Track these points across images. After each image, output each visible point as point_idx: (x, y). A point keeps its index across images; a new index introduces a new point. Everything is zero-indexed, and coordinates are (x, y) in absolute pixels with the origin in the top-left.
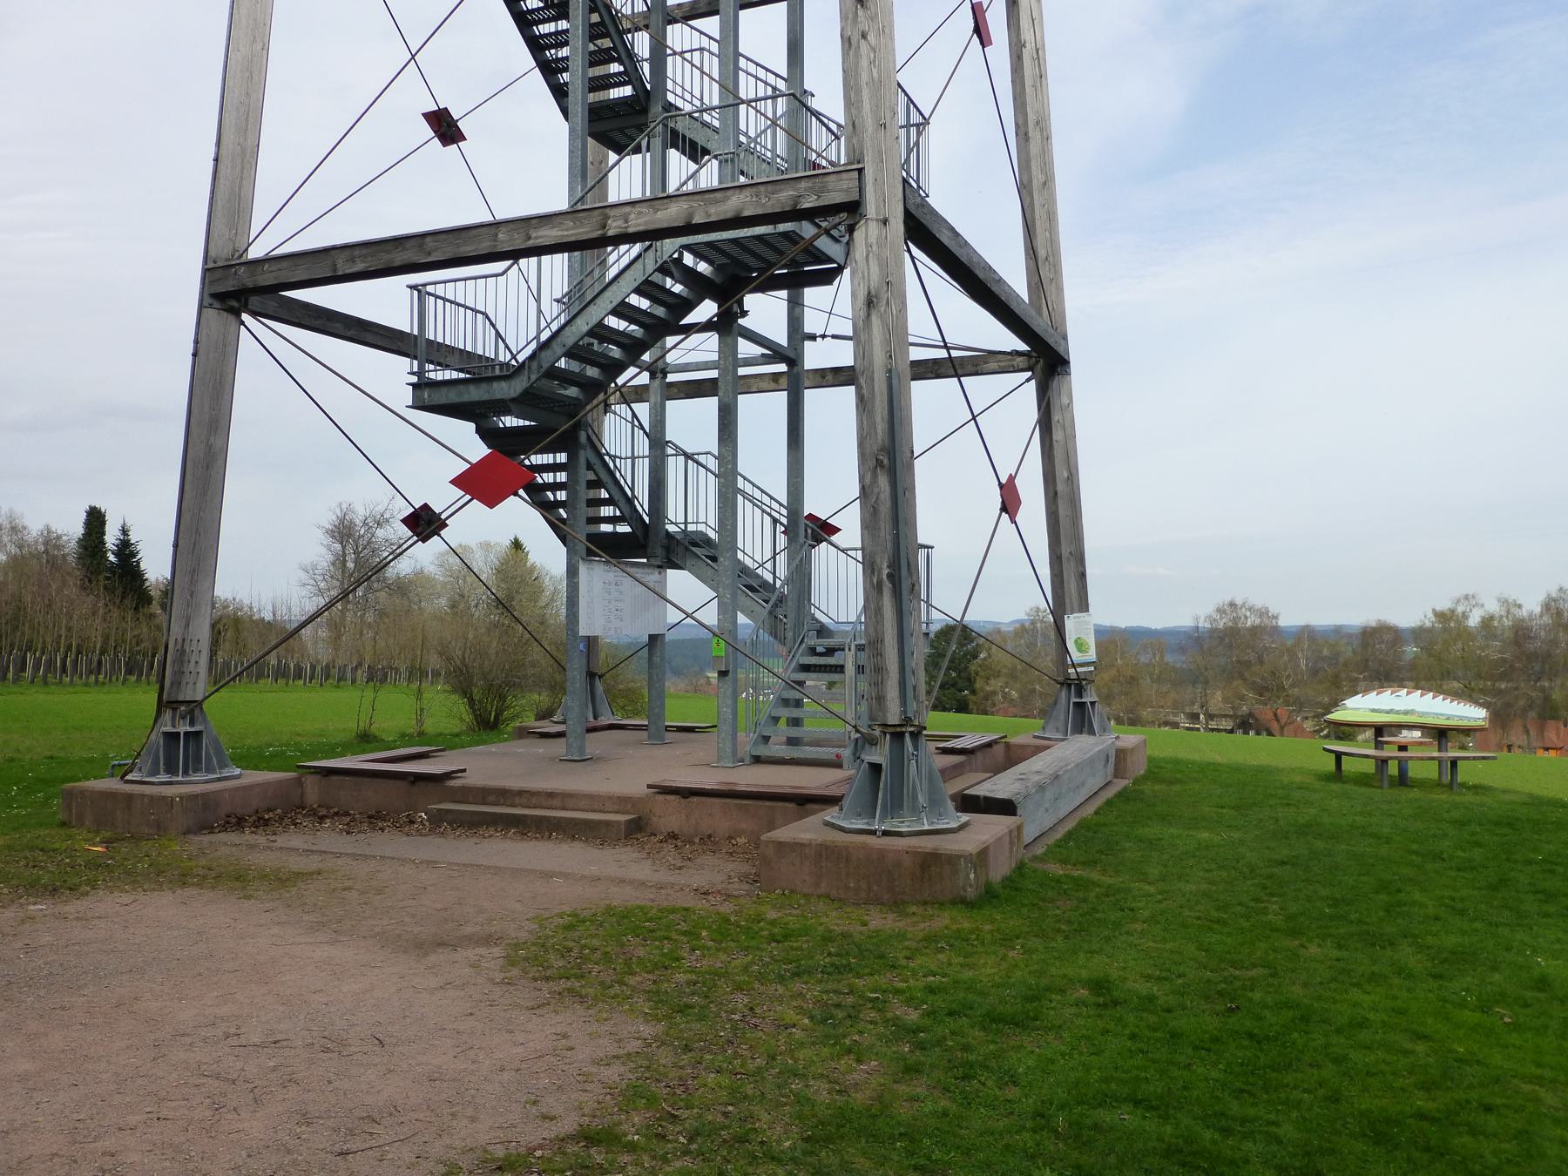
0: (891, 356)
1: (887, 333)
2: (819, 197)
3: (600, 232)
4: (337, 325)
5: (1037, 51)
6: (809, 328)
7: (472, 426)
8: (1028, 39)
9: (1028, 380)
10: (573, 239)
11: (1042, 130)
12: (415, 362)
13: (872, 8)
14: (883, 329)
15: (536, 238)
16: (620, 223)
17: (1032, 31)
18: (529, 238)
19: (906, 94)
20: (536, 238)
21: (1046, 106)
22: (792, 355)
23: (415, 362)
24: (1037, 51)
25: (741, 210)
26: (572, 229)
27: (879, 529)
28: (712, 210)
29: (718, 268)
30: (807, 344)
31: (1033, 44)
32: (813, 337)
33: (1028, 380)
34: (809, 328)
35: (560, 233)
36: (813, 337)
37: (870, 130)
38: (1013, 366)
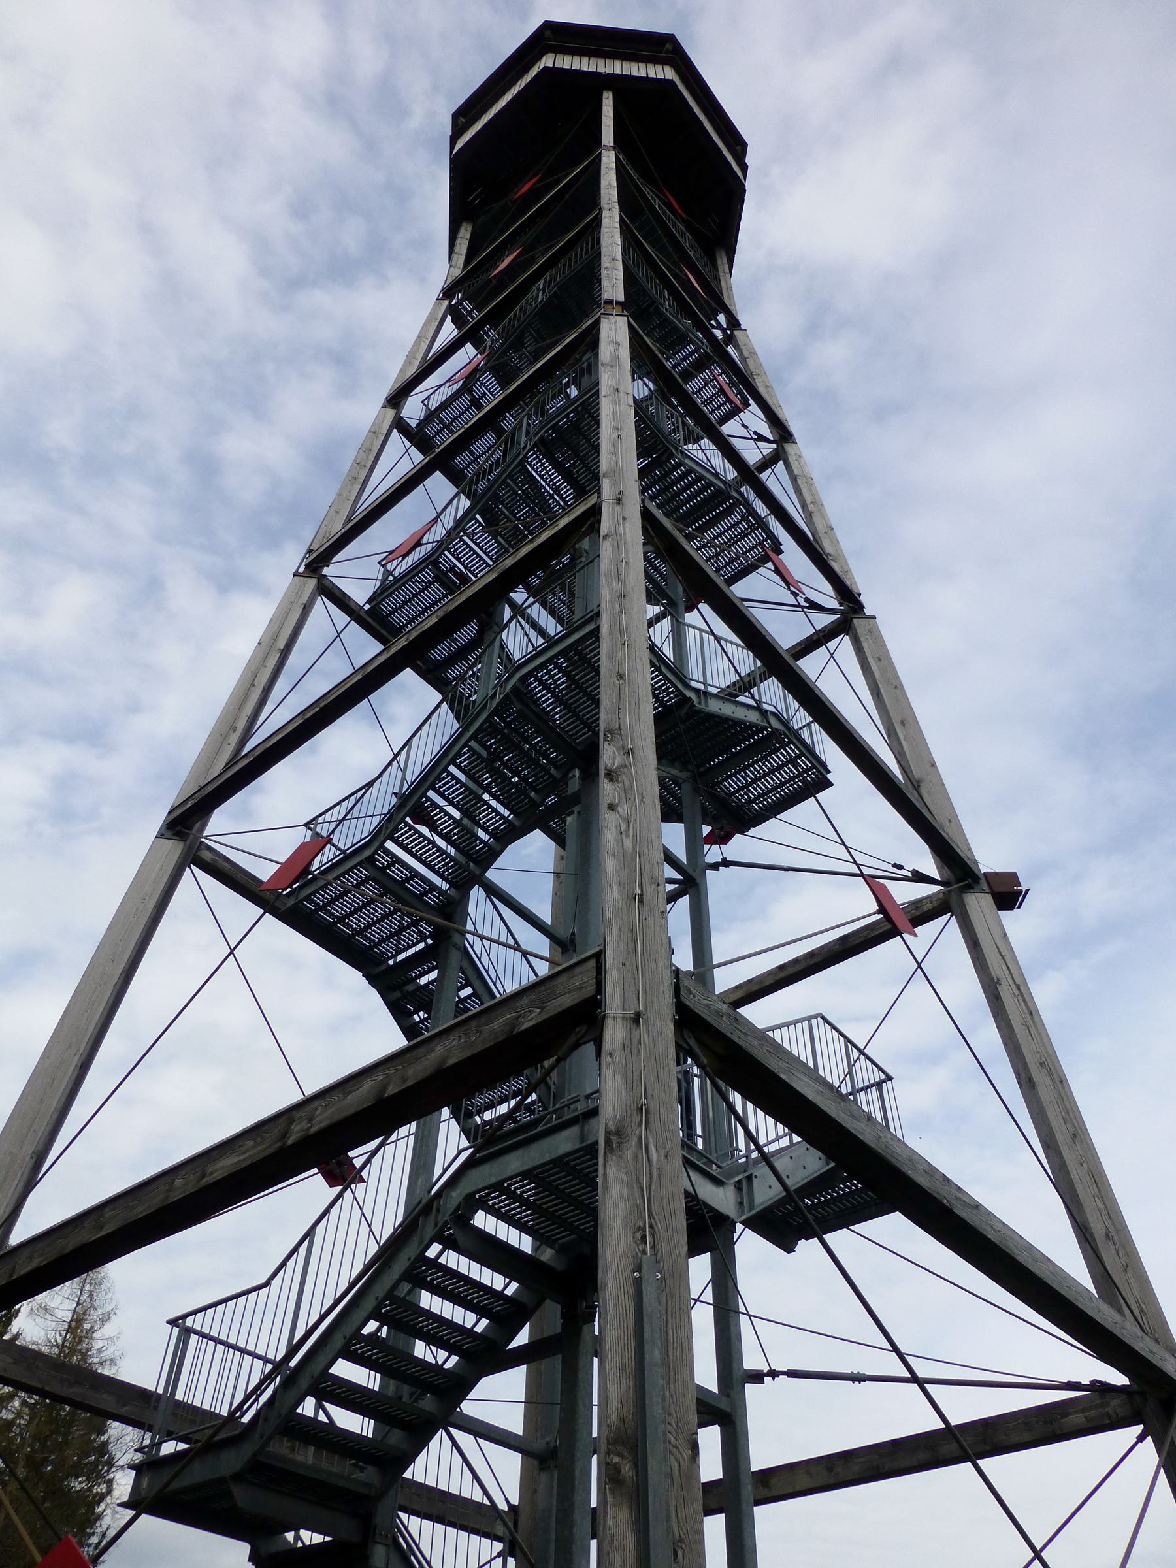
0: (644, 1237)
1: (637, 1194)
2: (543, 1008)
3: (279, 1144)
4: (105, 1396)
5: (1018, 987)
6: (752, 1361)
7: (244, 1548)
8: (1001, 975)
9: (1141, 1438)
10: (248, 1163)
11: (1050, 1073)
12: (148, 1435)
13: (626, 781)
14: (630, 1188)
15: (211, 1173)
16: (304, 1125)
17: (1004, 967)
18: (204, 1176)
19: (841, 1034)
20: (211, 1173)
21: (1045, 1040)
22: (724, 1405)
23: (148, 1435)
24: (1018, 987)
25: (445, 1060)
26: (253, 1147)
27: (34, 1544)
28: (410, 1072)
29: (561, 1251)
30: (749, 1387)
31: (1010, 981)
32: (757, 1377)
33: (1141, 1438)
34: (752, 1361)
35: (236, 1159)
36: (757, 1377)
37: (616, 905)
38: (1108, 1414)
